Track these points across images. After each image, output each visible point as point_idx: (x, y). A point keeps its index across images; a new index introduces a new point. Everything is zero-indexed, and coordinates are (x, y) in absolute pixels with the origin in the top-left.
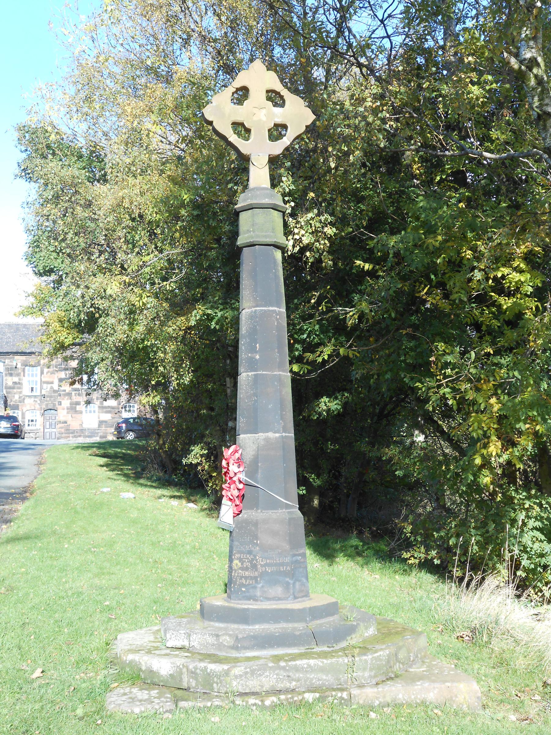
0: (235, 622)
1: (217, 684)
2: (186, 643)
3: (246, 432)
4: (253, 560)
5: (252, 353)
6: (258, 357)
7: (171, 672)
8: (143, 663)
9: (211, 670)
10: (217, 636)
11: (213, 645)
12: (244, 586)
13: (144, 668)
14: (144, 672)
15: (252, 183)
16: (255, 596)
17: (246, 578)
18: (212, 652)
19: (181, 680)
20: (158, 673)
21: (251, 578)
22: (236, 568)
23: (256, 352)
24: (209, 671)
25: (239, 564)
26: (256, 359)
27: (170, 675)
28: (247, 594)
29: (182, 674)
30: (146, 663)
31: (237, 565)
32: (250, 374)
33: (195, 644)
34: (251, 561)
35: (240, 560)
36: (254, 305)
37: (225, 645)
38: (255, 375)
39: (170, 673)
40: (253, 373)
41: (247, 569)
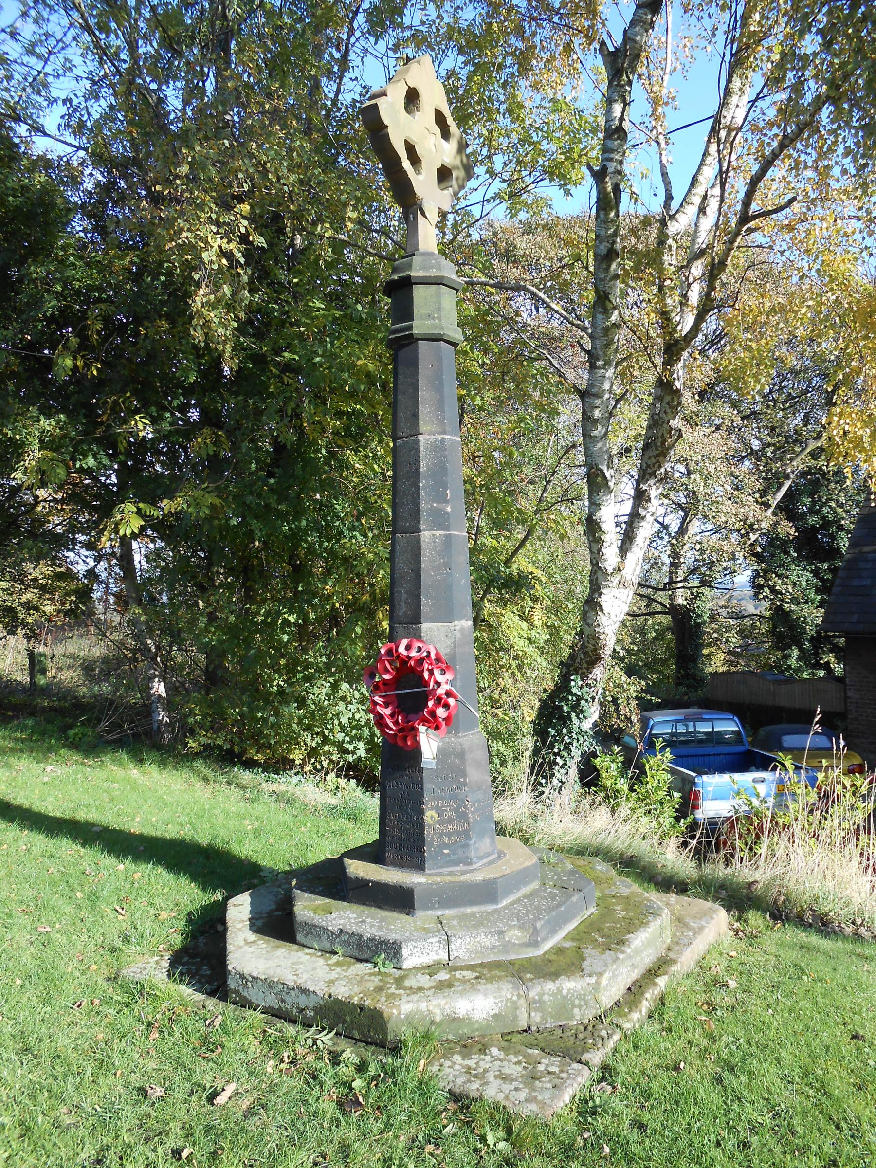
0: (473, 903)
1: (580, 1007)
2: (443, 955)
3: (432, 620)
4: (459, 806)
5: (438, 502)
6: (449, 509)
7: (496, 1011)
8: (437, 1012)
9: (569, 990)
10: (501, 933)
11: (494, 947)
12: (447, 846)
13: (438, 1019)
14: (439, 1025)
15: (422, 247)
16: (467, 857)
17: (449, 835)
18: (492, 958)
19: (515, 1018)
20: (470, 1019)
21: (459, 834)
22: (431, 822)
23: (446, 502)
24: (564, 992)
25: (436, 816)
26: (446, 513)
27: (495, 1016)
28: (453, 857)
29: (517, 1008)
30: (442, 1010)
31: (432, 817)
32: (438, 533)
33: (462, 954)
34: (456, 811)
35: (438, 809)
36: (439, 430)
37: (515, 944)
38: (446, 536)
39: (492, 1013)
40: (442, 533)
41: (450, 821)
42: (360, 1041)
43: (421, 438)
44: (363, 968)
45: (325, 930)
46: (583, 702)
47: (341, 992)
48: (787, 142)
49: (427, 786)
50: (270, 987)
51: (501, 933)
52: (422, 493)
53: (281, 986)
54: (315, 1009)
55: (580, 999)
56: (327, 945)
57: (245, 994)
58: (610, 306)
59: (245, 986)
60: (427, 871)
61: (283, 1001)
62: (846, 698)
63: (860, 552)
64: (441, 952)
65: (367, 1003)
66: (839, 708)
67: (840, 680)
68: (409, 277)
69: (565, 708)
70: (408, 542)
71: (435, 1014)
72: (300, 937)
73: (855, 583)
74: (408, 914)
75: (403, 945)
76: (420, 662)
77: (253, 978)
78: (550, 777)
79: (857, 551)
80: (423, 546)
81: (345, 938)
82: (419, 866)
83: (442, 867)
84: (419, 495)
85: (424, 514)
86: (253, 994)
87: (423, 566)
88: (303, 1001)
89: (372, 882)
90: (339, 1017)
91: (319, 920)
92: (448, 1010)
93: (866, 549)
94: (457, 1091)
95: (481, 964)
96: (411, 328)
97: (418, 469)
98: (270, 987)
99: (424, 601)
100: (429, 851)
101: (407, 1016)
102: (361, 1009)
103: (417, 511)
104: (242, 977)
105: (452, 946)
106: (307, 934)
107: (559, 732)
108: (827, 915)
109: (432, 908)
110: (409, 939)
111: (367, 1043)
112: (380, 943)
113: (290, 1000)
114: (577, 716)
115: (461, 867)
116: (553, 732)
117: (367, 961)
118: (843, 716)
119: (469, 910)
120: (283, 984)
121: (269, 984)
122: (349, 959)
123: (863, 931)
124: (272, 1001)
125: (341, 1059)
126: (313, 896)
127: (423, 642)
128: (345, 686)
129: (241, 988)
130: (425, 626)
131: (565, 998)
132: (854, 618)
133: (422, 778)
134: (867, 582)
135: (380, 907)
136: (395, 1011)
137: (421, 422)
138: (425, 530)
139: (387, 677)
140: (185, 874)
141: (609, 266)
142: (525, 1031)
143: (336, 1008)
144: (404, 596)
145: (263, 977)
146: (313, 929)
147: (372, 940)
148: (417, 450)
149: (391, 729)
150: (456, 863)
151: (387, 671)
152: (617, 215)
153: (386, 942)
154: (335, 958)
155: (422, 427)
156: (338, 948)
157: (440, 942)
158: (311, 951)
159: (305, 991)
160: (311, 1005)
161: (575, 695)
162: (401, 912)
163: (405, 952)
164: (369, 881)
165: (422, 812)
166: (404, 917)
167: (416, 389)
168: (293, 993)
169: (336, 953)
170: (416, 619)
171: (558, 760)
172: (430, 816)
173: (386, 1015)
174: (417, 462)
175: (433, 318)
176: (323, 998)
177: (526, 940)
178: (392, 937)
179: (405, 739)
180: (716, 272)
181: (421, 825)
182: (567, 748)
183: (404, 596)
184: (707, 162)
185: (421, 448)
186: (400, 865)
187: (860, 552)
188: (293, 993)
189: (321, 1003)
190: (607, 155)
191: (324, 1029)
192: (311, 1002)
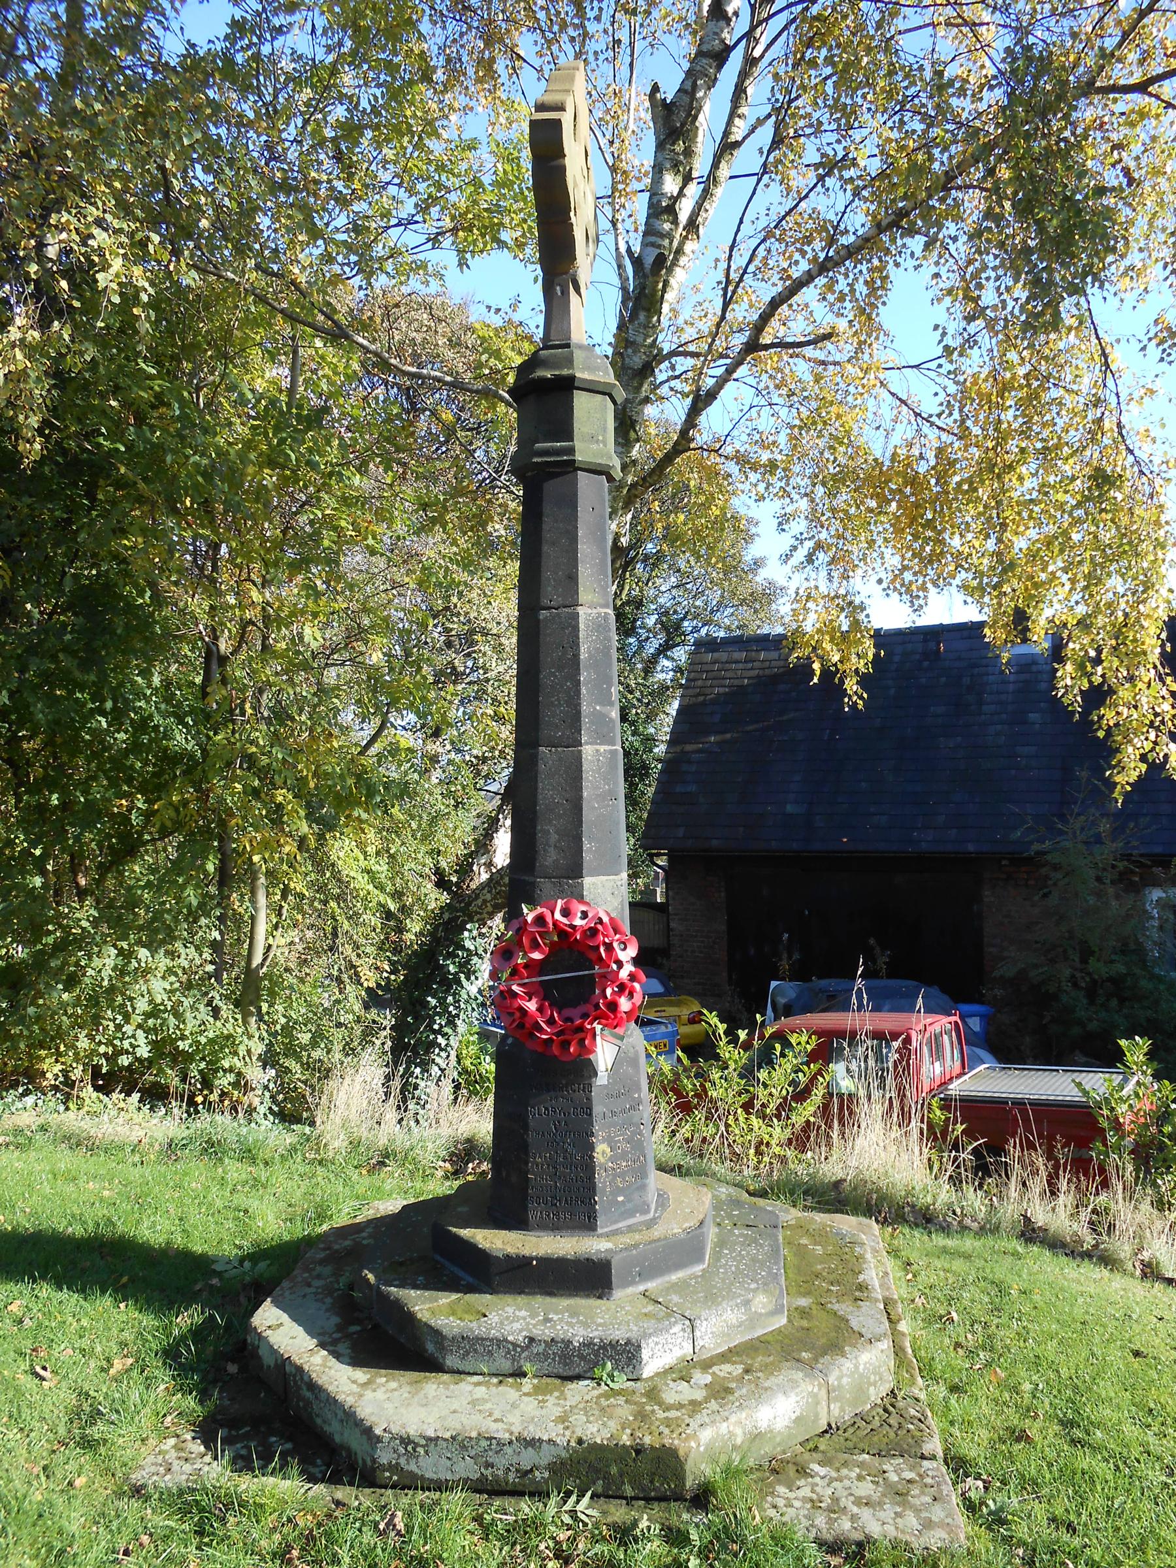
3: (596, 873)
4: (634, 1133)
7: (798, 1413)
8: (739, 1431)
22: (602, 1160)
28: (629, 1206)
29: (818, 1403)
32: (602, 748)
40: (607, 748)
42: (636, 1498)
43: (581, 611)
44: (580, 1390)
45: (501, 1342)
46: (475, 959)
47: (597, 1431)
48: (829, 265)
49: (598, 1109)
50: (464, 1447)
51: (747, 1303)
52: (584, 691)
53: (484, 1443)
54: (551, 1468)
55: (874, 1373)
56: (506, 1365)
57: (412, 1467)
58: (632, 435)
59: (413, 1455)
60: (600, 1231)
61: (488, 1465)
62: (669, 929)
63: (682, 751)
64: (685, 1344)
65: (647, 1440)
66: (657, 942)
67: (661, 908)
68: (572, 378)
69: (452, 969)
70: (560, 759)
71: (735, 1435)
72: (451, 1361)
73: (679, 789)
74: (600, 1297)
75: (643, 1345)
76: (593, 932)
77: (430, 1439)
78: (425, 1066)
79: (678, 749)
80: (585, 766)
81: (538, 1349)
82: (587, 1223)
83: (616, 1222)
84: (578, 692)
85: (585, 720)
86: (428, 1466)
87: (585, 794)
88: (527, 1458)
89: (536, 1258)
90: (597, 1471)
91: (477, 1328)
92: (749, 1427)
93: (689, 748)
94: (829, 1537)
95: (730, 1350)
96: (571, 451)
97: (576, 656)
98: (464, 1447)
99: (586, 845)
100: (601, 1200)
101: (709, 1447)
102: (638, 1452)
103: (576, 717)
104: (406, 1441)
105: (698, 1334)
106: (467, 1353)
107: (442, 1002)
108: (928, 1208)
109: (632, 1283)
110: (646, 1336)
111: (648, 1500)
112: (603, 1347)
113: (501, 1462)
114: (468, 979)
115: (639, 1218)
116: (433, 1002)
117: (579, 1377)
118: (665, 952)
119: (674, 1277)
120: (490, 1439)
121: (460, 1443)
122: (545, 1380)
123: (968, 1221)
124: (467, 1468)
125: (638, 1532)
126: (434, 1293)
127: (588, 904)
128: (143, 953)
129: (402, 1461)
130: (588, 881)
131: (861, 1376)
132: (681, 832)
133: (589, 1099)
134: (693, 788)
135: (551, 1294)
136: (693, 1444)
137: (581, 589)
138: (587, 743)
139: (537, 956)
140: (103, 1292)
141: (641, 385)
142: (826, 1432)
143: (592, 1457)
144: (554, 837)
145: (447, 1435)
146: (472, 1345)
147: (589, 1344)
148: (576, 628)
149: (546, 1033)
150: (631, 1214)
151: (536, 946)
152: (659, 321)
153: (614, 1345)
154: (528, 1384)
155: (584, 596)
156: (527, 1367)
157: (683, 1330)
158: (476, 1378)
159: (533, 1443)
160: (544, 1462)
161: (468, 950)
162: (588, 1296)
163: (645, 1354)
164: (532, 1259)
165: (592, 1148)
166: (593, 1302)
167: (574, 539)
168: (508, 1450)
169: (524, 1375)
170: (575, 870)
171: (440, 1040)
172: (602, 1152)
173: (681, 1453)
174: (575, 645)
175: (597, 441)
176: (566, 1448)
177: (771, 1307)
178: (619, 1334)
179: (565, 1045)
180: (700, 405)
181: (588, 1166)
182: (451, 1023)
183: (554, 837)
184: (681, 263)
185: (582, 626)
186: (555, 1227)
187: (682, 751)
188: (508, 1450)
189: (564, 1454)
190: (652, 239)
191: (568, 1494)
192: (546, 1456)
